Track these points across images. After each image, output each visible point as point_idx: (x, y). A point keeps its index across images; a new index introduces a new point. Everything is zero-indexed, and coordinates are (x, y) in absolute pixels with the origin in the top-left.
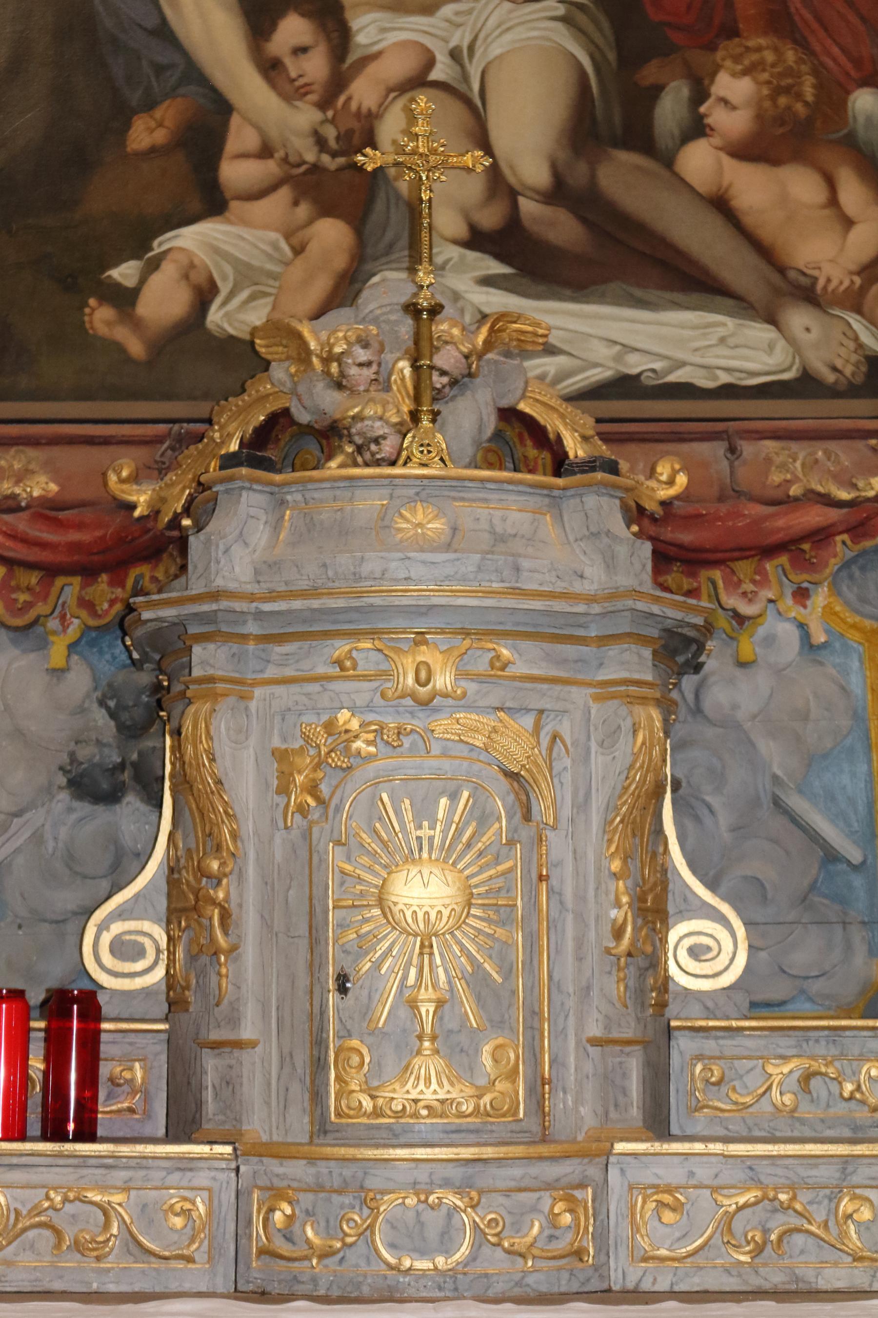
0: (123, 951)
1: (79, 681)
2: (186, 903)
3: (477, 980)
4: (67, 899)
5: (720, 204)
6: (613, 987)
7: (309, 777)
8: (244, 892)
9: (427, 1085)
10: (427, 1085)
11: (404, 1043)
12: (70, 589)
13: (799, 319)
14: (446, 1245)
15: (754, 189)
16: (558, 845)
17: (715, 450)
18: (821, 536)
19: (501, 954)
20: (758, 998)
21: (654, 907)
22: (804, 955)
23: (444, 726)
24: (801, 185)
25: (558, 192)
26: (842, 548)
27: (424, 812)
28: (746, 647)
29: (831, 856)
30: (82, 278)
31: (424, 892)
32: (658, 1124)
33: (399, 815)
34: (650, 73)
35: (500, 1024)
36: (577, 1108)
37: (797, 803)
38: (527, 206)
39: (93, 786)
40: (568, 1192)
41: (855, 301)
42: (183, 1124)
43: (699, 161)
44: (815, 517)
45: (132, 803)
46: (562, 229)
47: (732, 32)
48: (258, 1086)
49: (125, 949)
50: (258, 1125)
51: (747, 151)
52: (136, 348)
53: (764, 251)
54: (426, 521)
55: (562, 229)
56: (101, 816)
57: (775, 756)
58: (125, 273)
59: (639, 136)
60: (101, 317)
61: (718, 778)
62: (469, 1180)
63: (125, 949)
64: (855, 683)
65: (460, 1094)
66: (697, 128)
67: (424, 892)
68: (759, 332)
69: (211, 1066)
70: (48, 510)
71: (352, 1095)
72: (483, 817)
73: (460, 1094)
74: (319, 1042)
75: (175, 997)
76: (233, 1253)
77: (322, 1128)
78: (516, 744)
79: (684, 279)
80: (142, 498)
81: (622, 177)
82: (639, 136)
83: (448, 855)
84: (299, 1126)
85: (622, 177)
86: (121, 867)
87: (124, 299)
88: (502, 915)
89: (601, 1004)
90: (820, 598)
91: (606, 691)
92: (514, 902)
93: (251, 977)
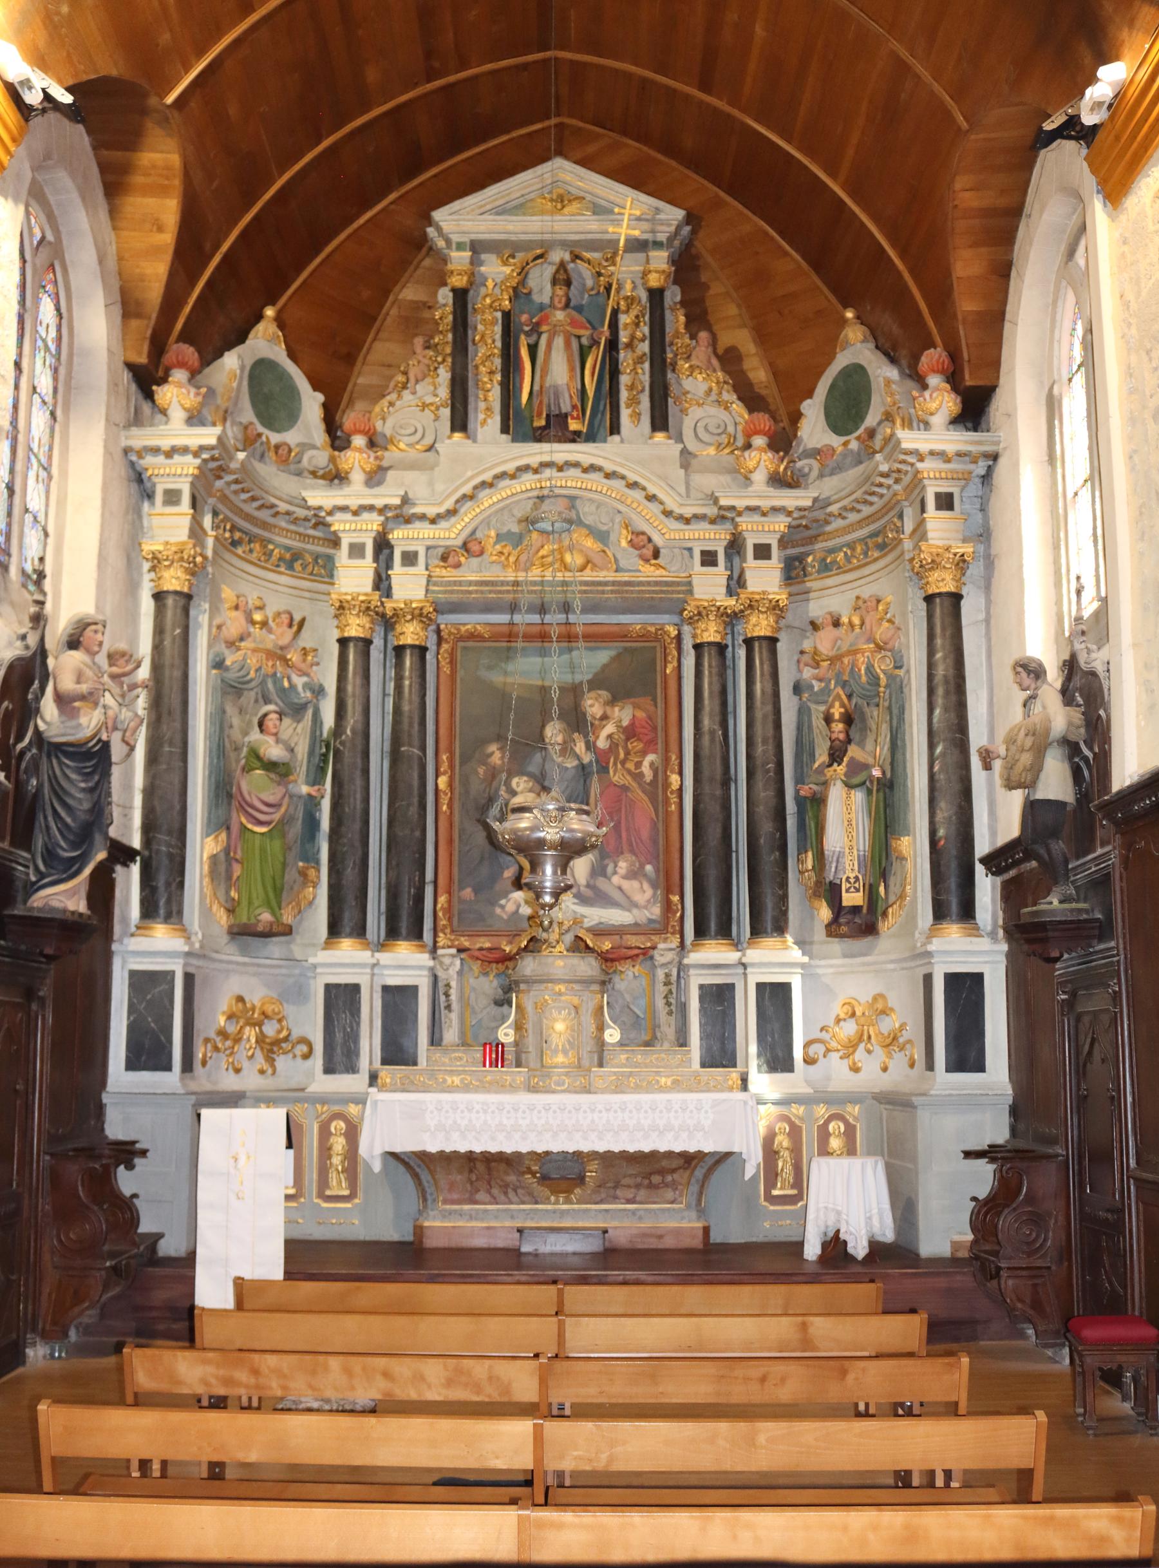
0: (506, 1035)
1: (495, 983)
2: (519, 1027)
3: (569, 1042)
4: (494, 1024)
5: (620, 888)
6: (592, 1042)
7: (541, 1007)
8: (529, 1026)
9: (560, 1059)
10: (560, 1059)
11: (556, 1051)
12: (494, 965)
13: (635, 911)
14: (563, 1084)
15: (626, 885)
16: (582, 1018)
17: (617, 937)
18: (637, 956)
19: (573, 1037)
20: (621, 1044)
21: (601, 1028)
22: (632, 1036)
23: (563, 998)
24: (635, 884)
25: (588, 886)
26: (641, 957)
27: (560, 1013)
28: (623, 976)
29: (638, 1017)
30: (493, 903)
31: (560, 1026)
32: (601, 1065)
33: (555, 1013)
34: (606, 862)
35: (572, 1048)
36: (586, 1063)
37: (632, 1007)
38: (582, 888)
39: (499, 1003)
40: (584, 1076)
41: (646, 907)
42: (518, 1065)
43: (616, 879)
44: (636, 951)
45: (506, 1007)
46: (588, 893)
47: (622, 853)
48: (532, 1058)
49: (506, 1035)
50: (532, 1065)
51: (625, 877)
52: (505, 917)
53: (628, 898)
54: (560, 963)
55: (588, 893)
56: (500, 1009)
57: (628, 997)
58: (503, 902)
59: (604, 874)
60: (498, 911)
61: (617, 1002)
62: (567, 1074)
63: (506, 1035)
64: (644, 983)
65: (565, 1060)
66: (615, 873)
67: (560, 1026)
68: (627, 914)
69: (523, 1056)
70: (489, 949)
71: (548, 1061)
72: (569, 1014)
73: (565, 1060)
74: (542, 1052)
75: (516, 1044)
76: (347, 1486)
77: (542, 1066)
78: (576, 1001)
79: (615, 904)
80: (508, 949)
81: (601, 883)
82: (604, 874)
83: (564, 1020)
84: (539, 1065)
85: (601, 883)
86: (504, 1019)
87: (503, 907)
88: (573, 1030)
89: (589, 1045)
90: (637, 967)
91: (592, 992)
92: (576, 1029)
93: (530, 1041)
